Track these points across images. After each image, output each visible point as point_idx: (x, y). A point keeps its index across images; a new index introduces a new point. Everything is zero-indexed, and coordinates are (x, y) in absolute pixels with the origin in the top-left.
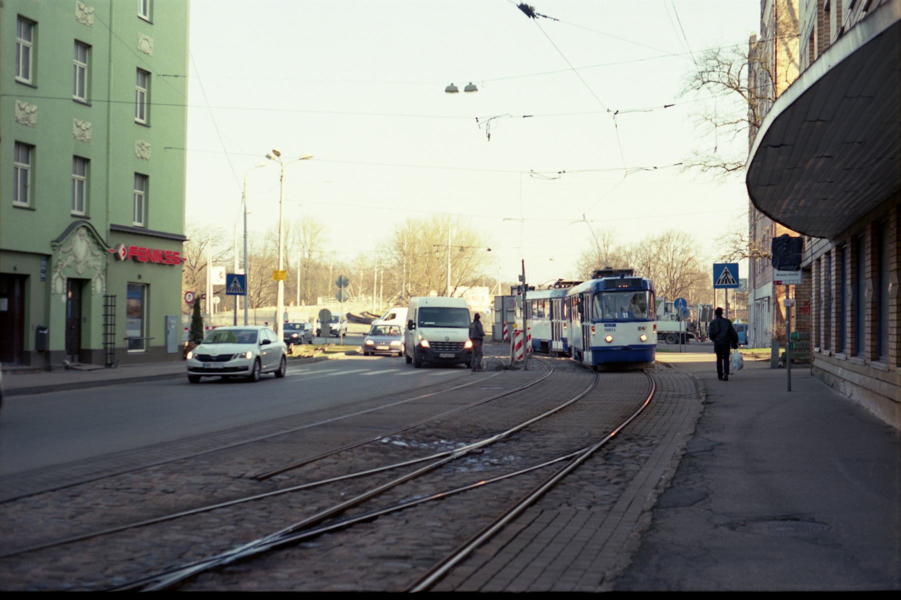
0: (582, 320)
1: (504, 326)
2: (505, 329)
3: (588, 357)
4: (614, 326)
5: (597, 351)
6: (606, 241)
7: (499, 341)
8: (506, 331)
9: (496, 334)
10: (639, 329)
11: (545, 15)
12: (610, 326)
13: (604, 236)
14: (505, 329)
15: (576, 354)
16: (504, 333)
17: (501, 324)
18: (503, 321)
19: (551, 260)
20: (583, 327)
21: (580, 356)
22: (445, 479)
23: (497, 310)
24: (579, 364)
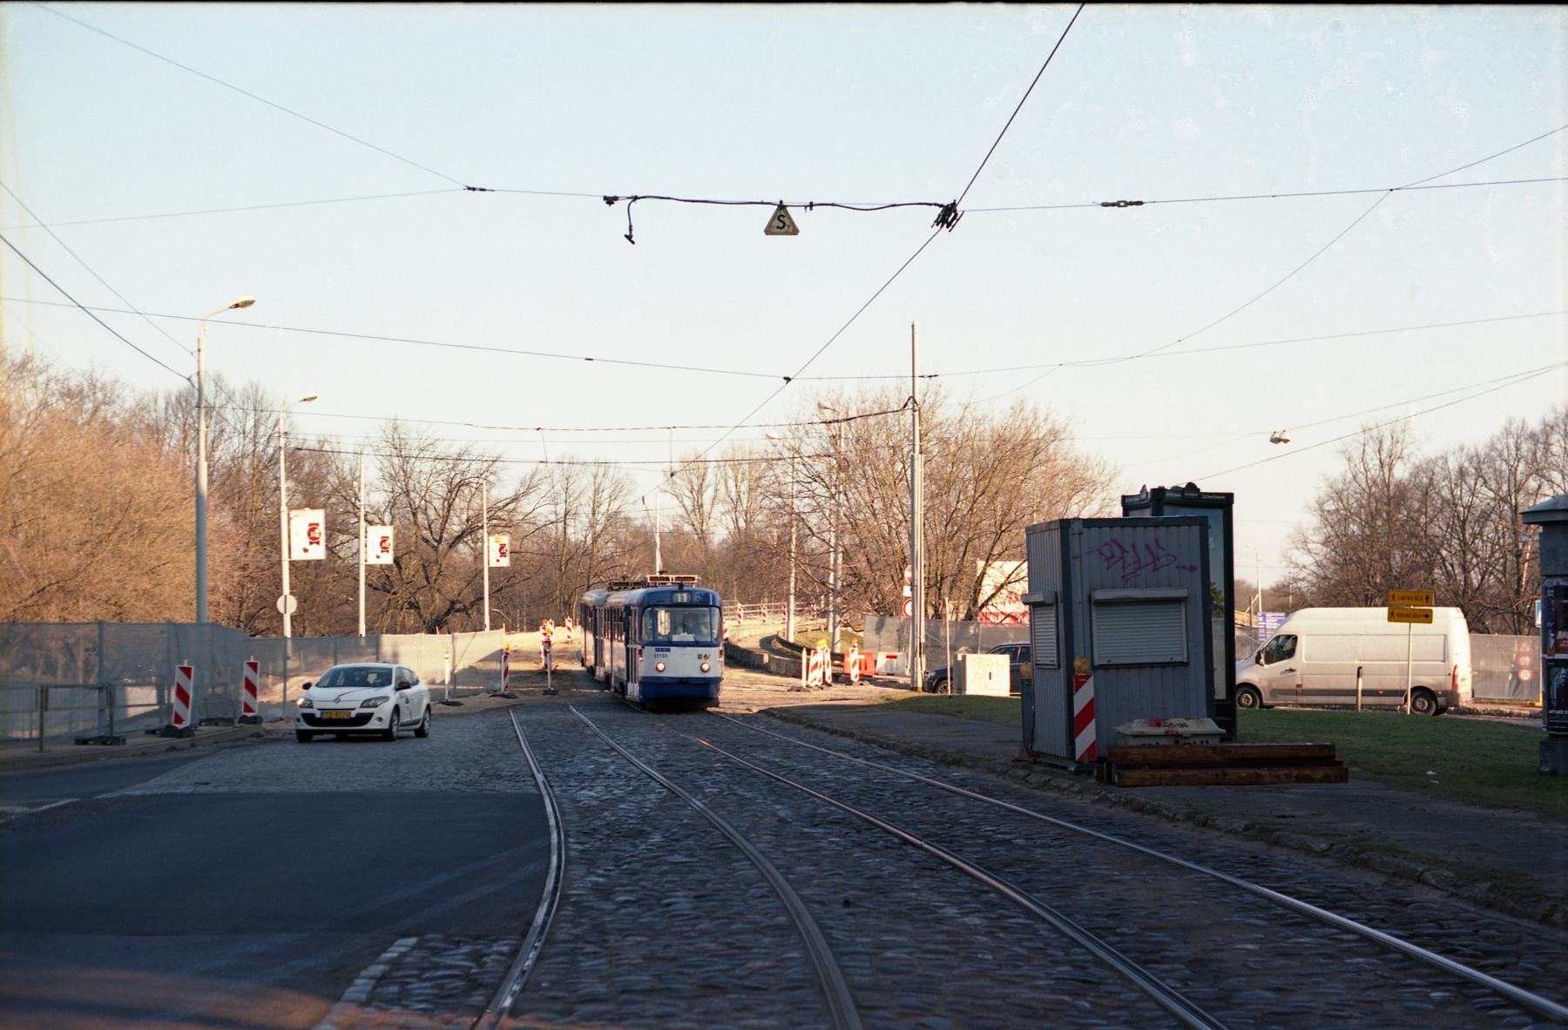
0: (627, 642)
1: (1073, 683)
2: (1082, 698)
3: (634, 690)
4: (668, 650)
5: (647, 683)
6: (1384, 455)
7: (1054, 766)
8: (1089, 712)
9: (1040, 729)
10: (700, 657)
11: (483, 187)
12: (662, 650)
13: (1381, 442)
14: (1082, 698)
15: (618, 685)
16: (1075, 725)
17: (1062, 673)
18: (1070, 657)
19: (1276, 441)
20: (628, 649)
21: (623, 687)
22: (178, 785)
23: (1039, 598)
24: (620, 700)
